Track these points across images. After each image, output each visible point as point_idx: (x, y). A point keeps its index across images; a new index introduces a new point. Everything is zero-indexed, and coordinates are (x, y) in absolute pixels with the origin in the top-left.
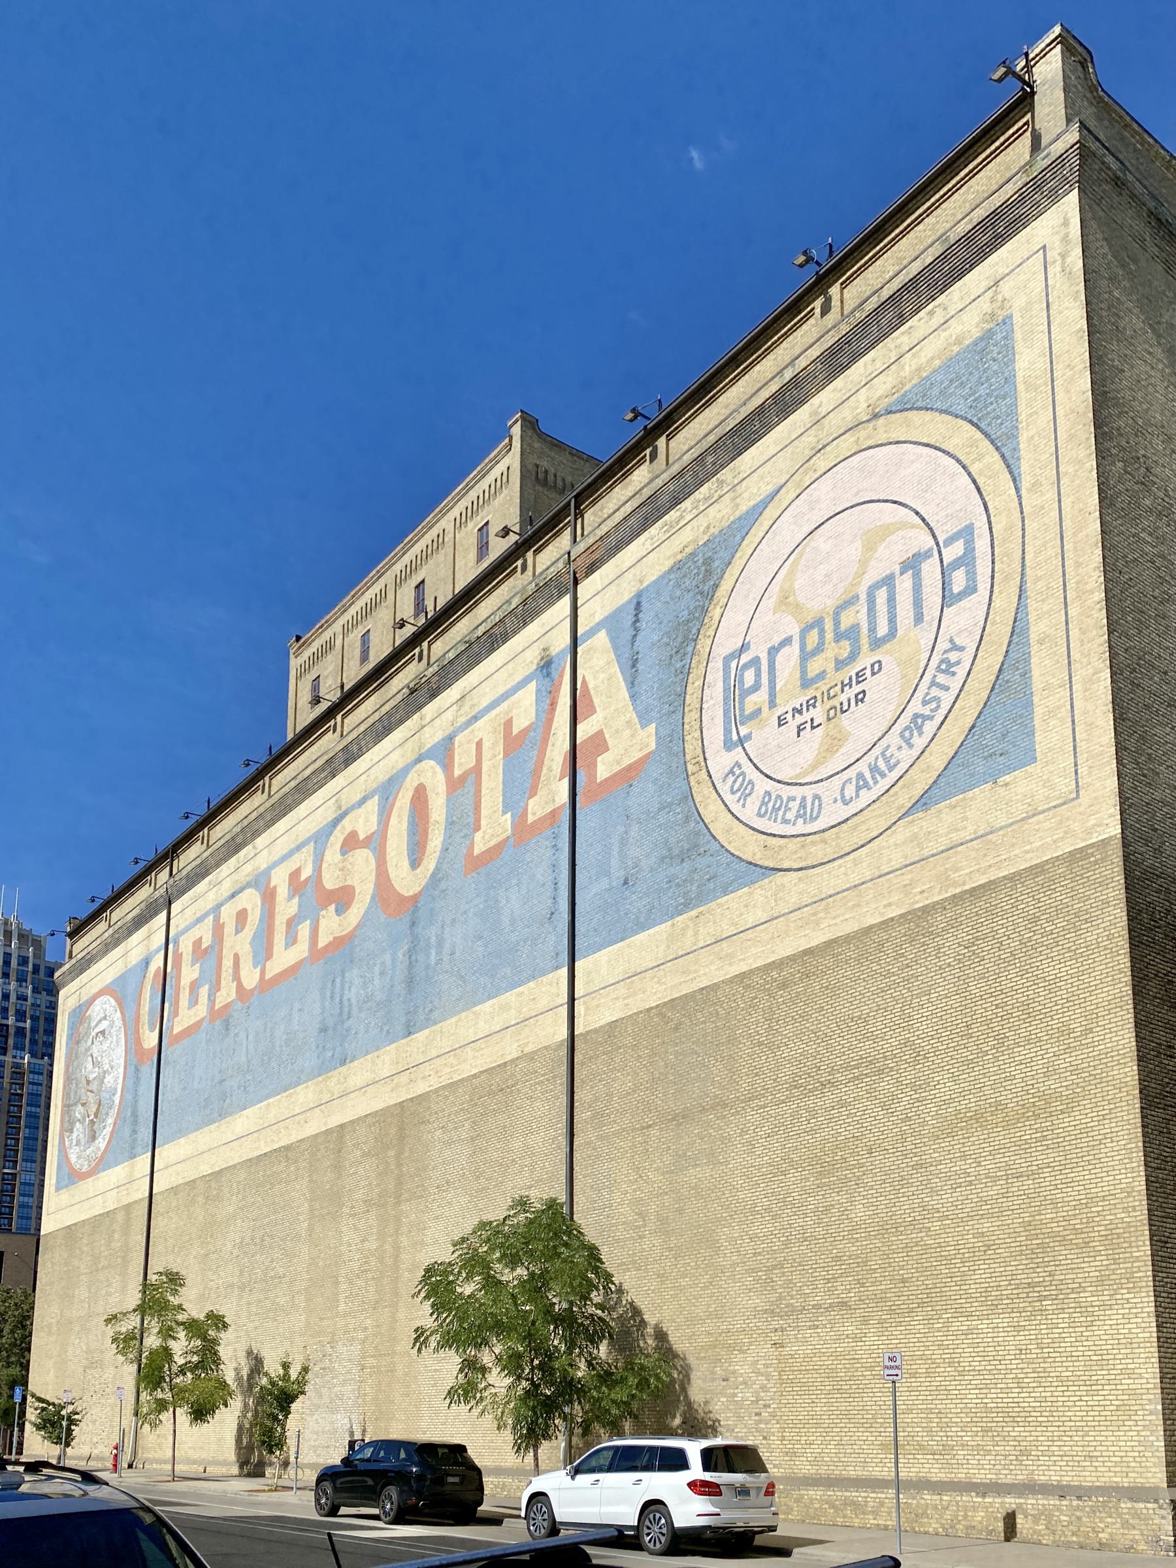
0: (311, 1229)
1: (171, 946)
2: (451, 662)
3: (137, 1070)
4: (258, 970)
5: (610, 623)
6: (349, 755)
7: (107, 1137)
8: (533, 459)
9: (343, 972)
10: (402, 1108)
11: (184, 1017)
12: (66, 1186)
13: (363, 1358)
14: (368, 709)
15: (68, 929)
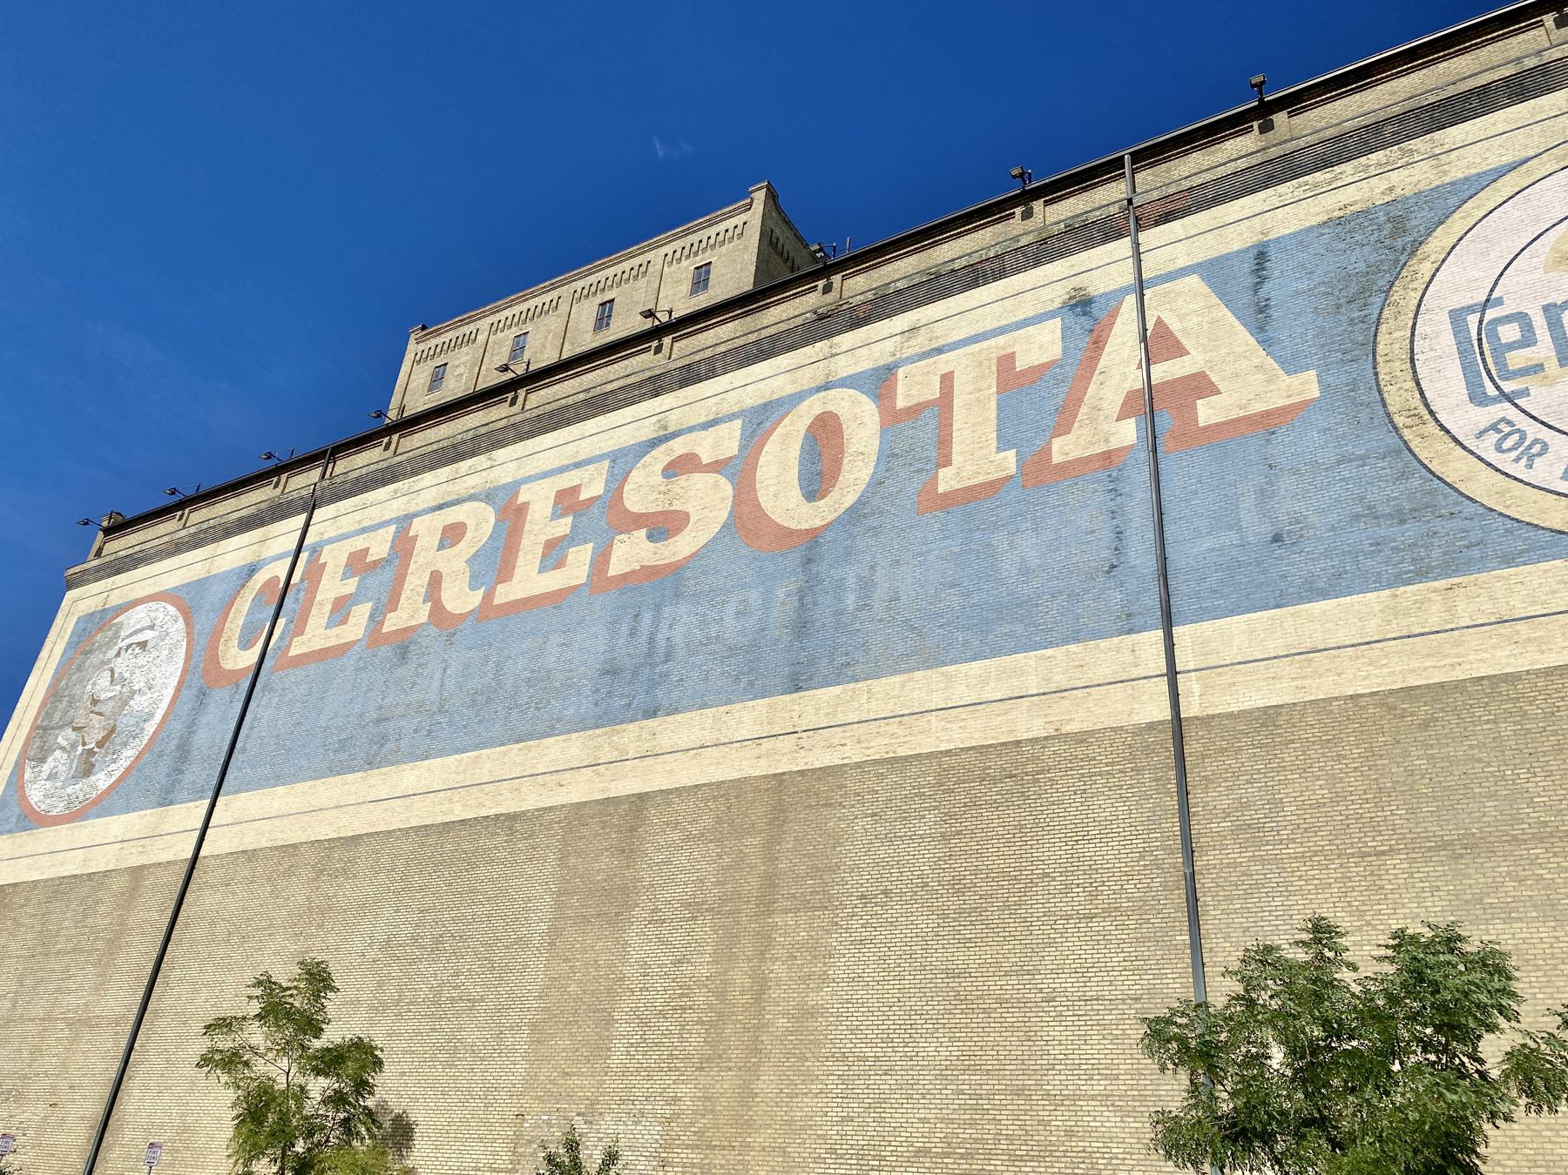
0: (554, 934)
1: (304, 556)
2: (899, 292)
3: (203, 694)
4: (480, 593)
6: (690, 375)
7: (117, 774)
8: (770, 224)
9: (658, 608)
10: (781, 782)
12: (10, 832)
13: (668, 1147)
14: (642, 363)
15: (105, 524)
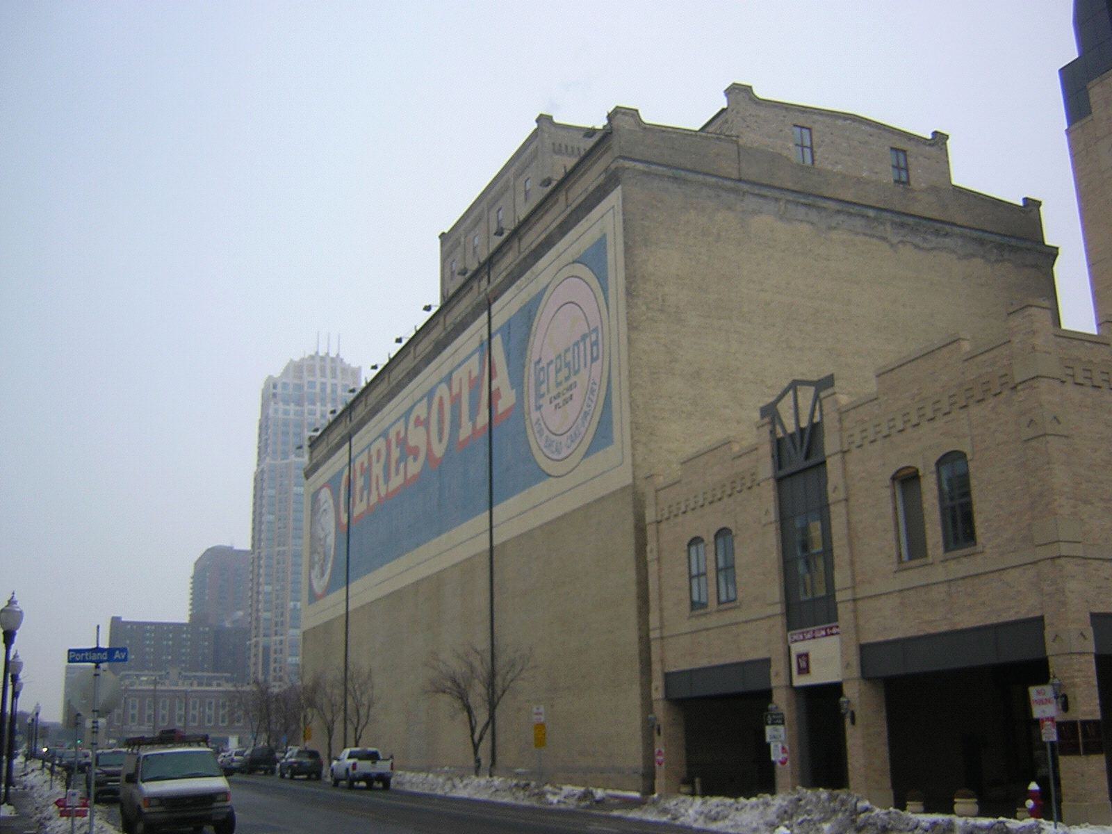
5: (500, 330)
11: (359, 508)
